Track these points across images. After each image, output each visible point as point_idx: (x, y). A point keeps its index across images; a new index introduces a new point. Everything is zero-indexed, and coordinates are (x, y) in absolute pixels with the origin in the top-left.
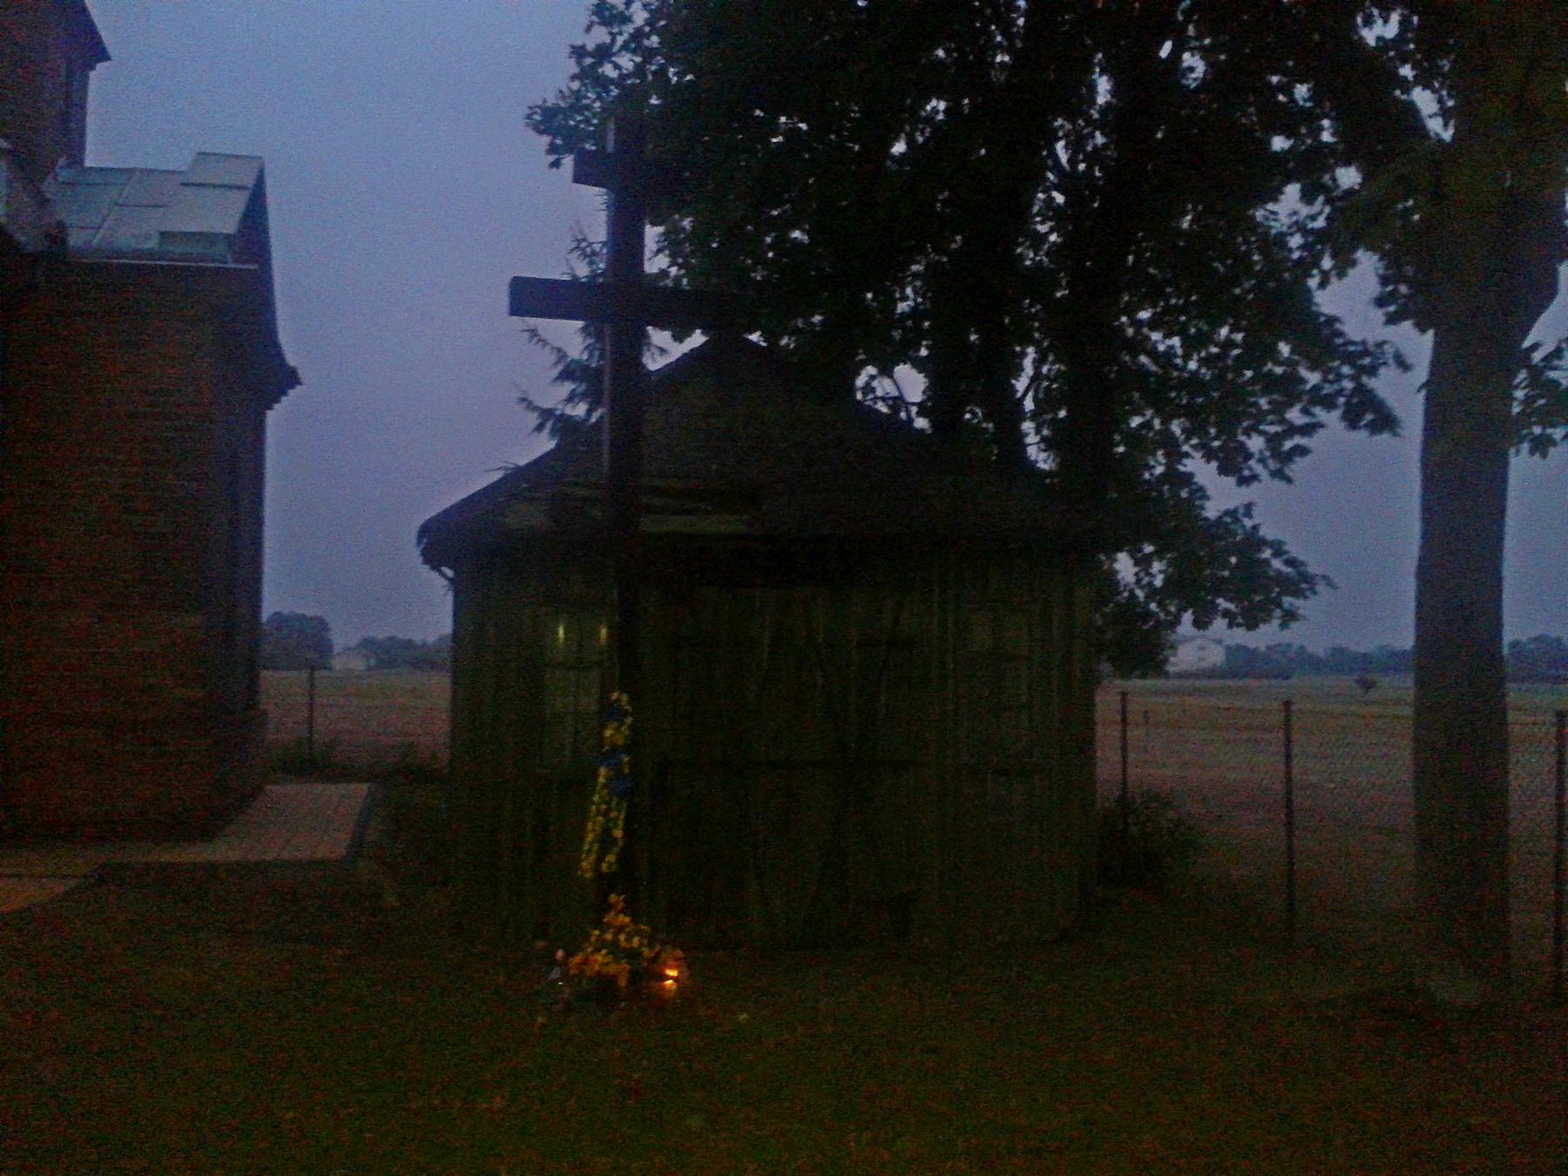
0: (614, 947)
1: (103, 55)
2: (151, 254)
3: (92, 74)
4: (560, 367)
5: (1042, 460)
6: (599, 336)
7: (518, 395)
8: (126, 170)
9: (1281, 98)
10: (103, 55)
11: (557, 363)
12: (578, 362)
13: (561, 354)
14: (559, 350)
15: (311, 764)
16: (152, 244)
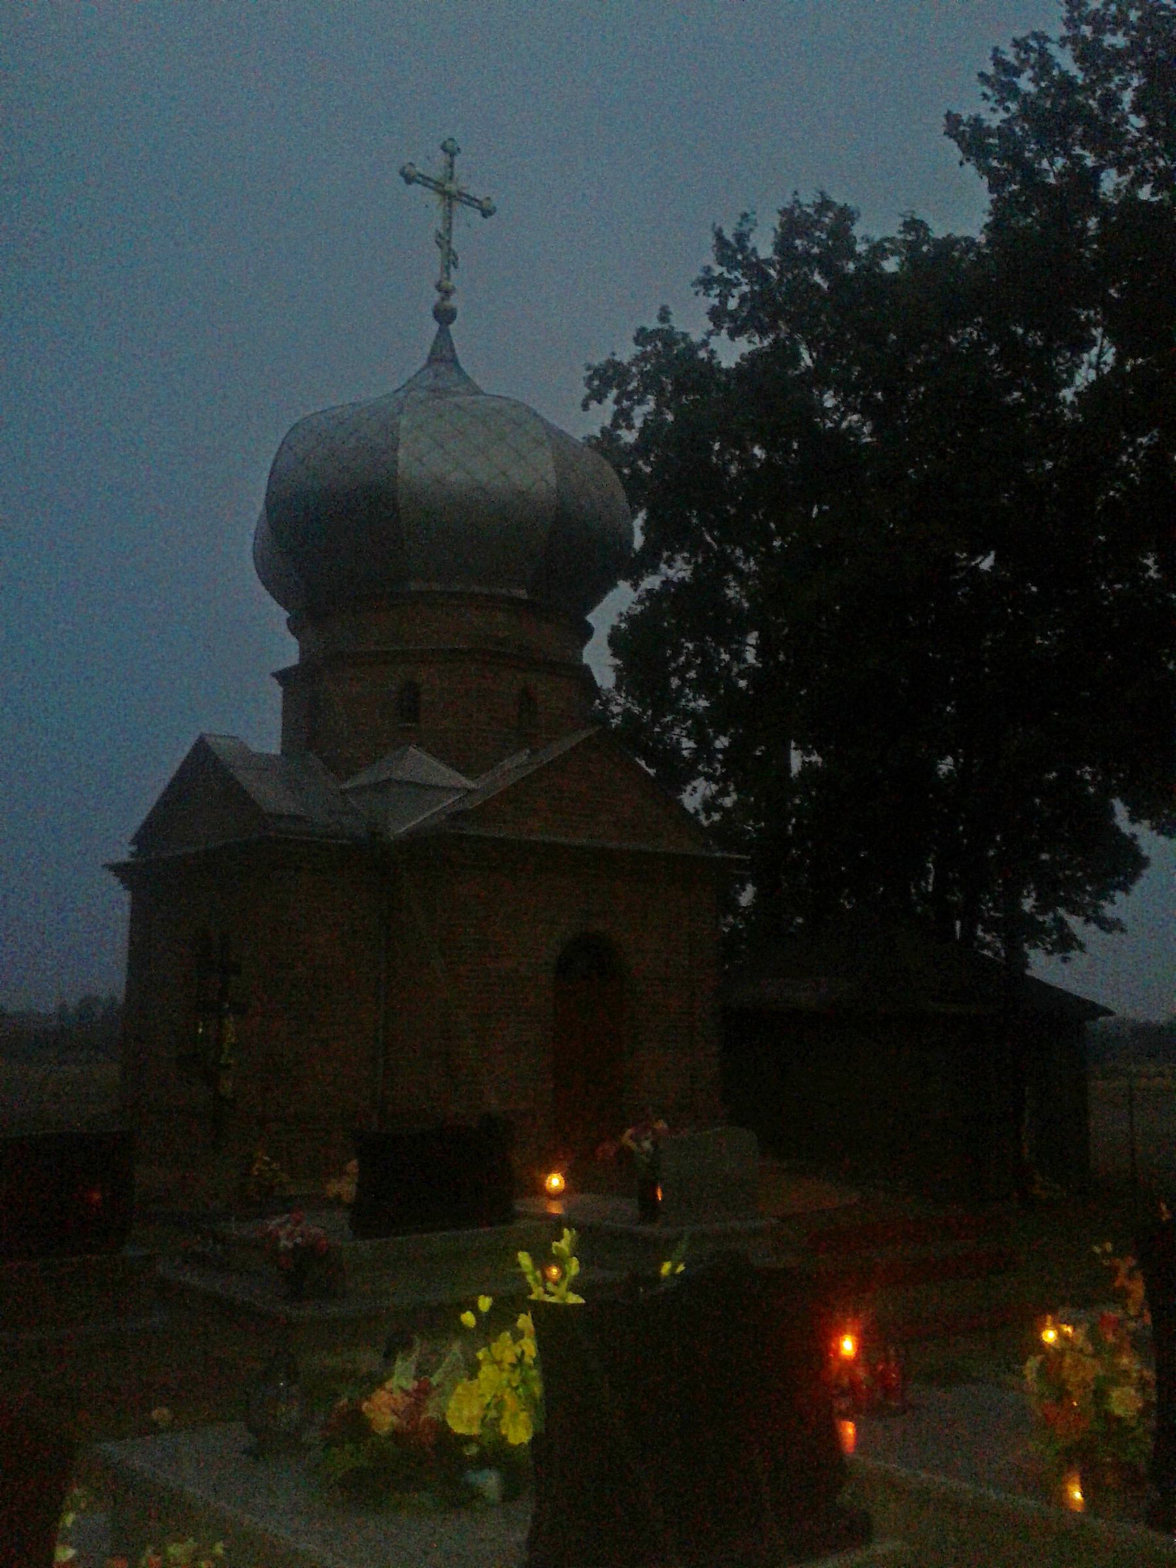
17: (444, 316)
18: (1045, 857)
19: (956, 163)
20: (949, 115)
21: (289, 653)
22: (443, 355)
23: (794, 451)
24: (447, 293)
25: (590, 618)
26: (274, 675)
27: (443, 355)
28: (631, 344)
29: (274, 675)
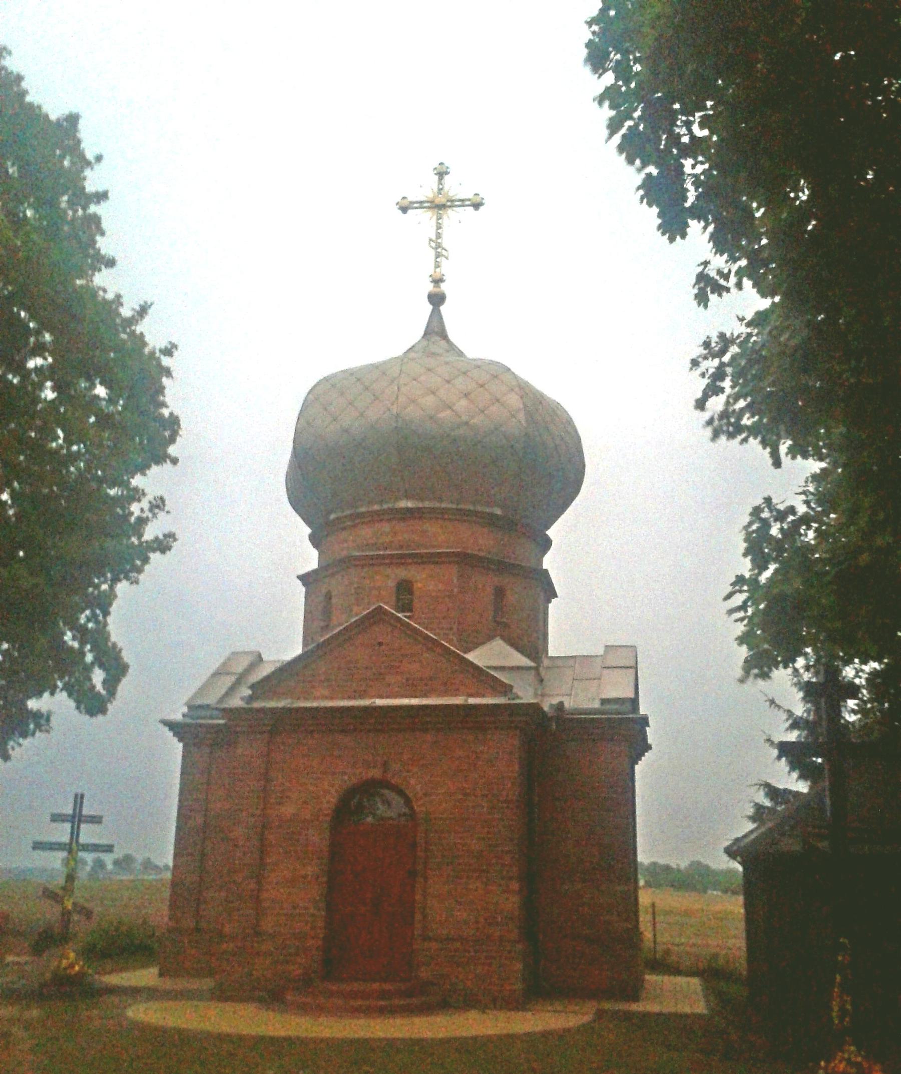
0: (849, 1061)
1: (555, 596)
2: (596, 711)
3: (550, 605)
4: (790, 722)
5: (60, 433)
6: (816, 704)
7: (765, 737)
8: (572, 657)
9: (824, 528)
10: (555, 596)
11: (787, 720)
12: (801, 718)
13: (790, 713)
14: (789, 711)
15: (662, 964)
16: (596, 705)
17: (437, 299)
18: (840, 470)
19: (169, 516)
20: (706, 306)
21: (311, 559)
22: (436, 330)
23: (790, 192)
24: (437, 281)
25: (550, 533)
26: (299, 577)
27: (436, 330)
28: (152, 560)
29: (299, 577)
